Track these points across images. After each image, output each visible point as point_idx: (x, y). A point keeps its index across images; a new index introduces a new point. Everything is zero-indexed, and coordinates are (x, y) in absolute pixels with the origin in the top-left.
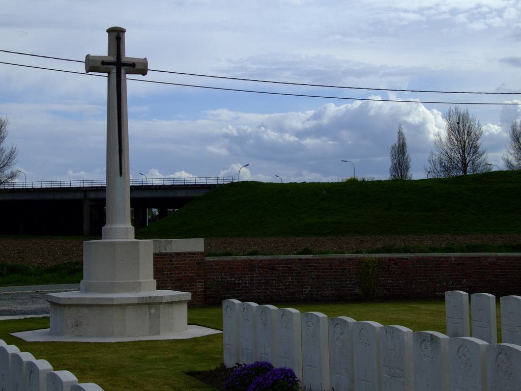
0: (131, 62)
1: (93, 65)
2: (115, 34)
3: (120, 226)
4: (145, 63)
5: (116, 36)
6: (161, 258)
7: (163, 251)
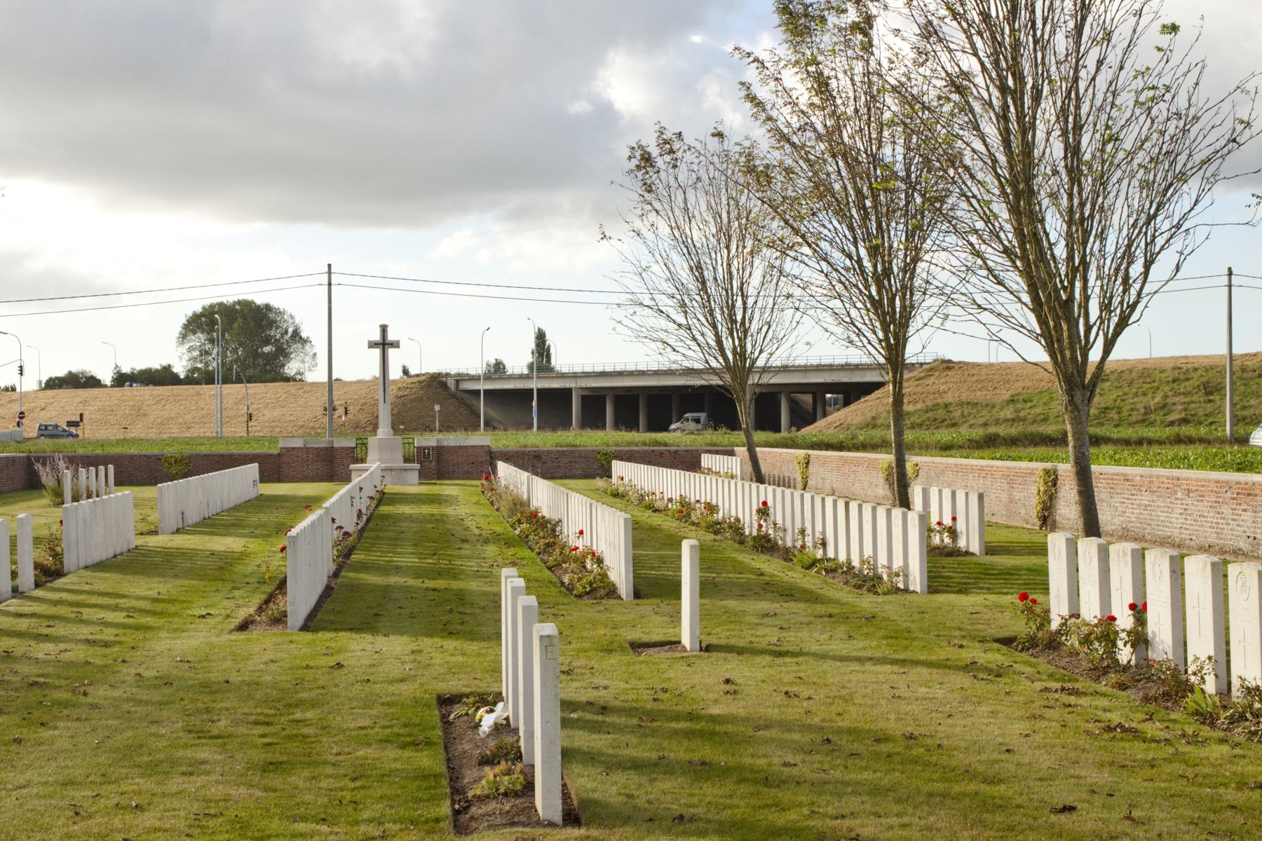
1: (372, 345)
5: (384, 329)
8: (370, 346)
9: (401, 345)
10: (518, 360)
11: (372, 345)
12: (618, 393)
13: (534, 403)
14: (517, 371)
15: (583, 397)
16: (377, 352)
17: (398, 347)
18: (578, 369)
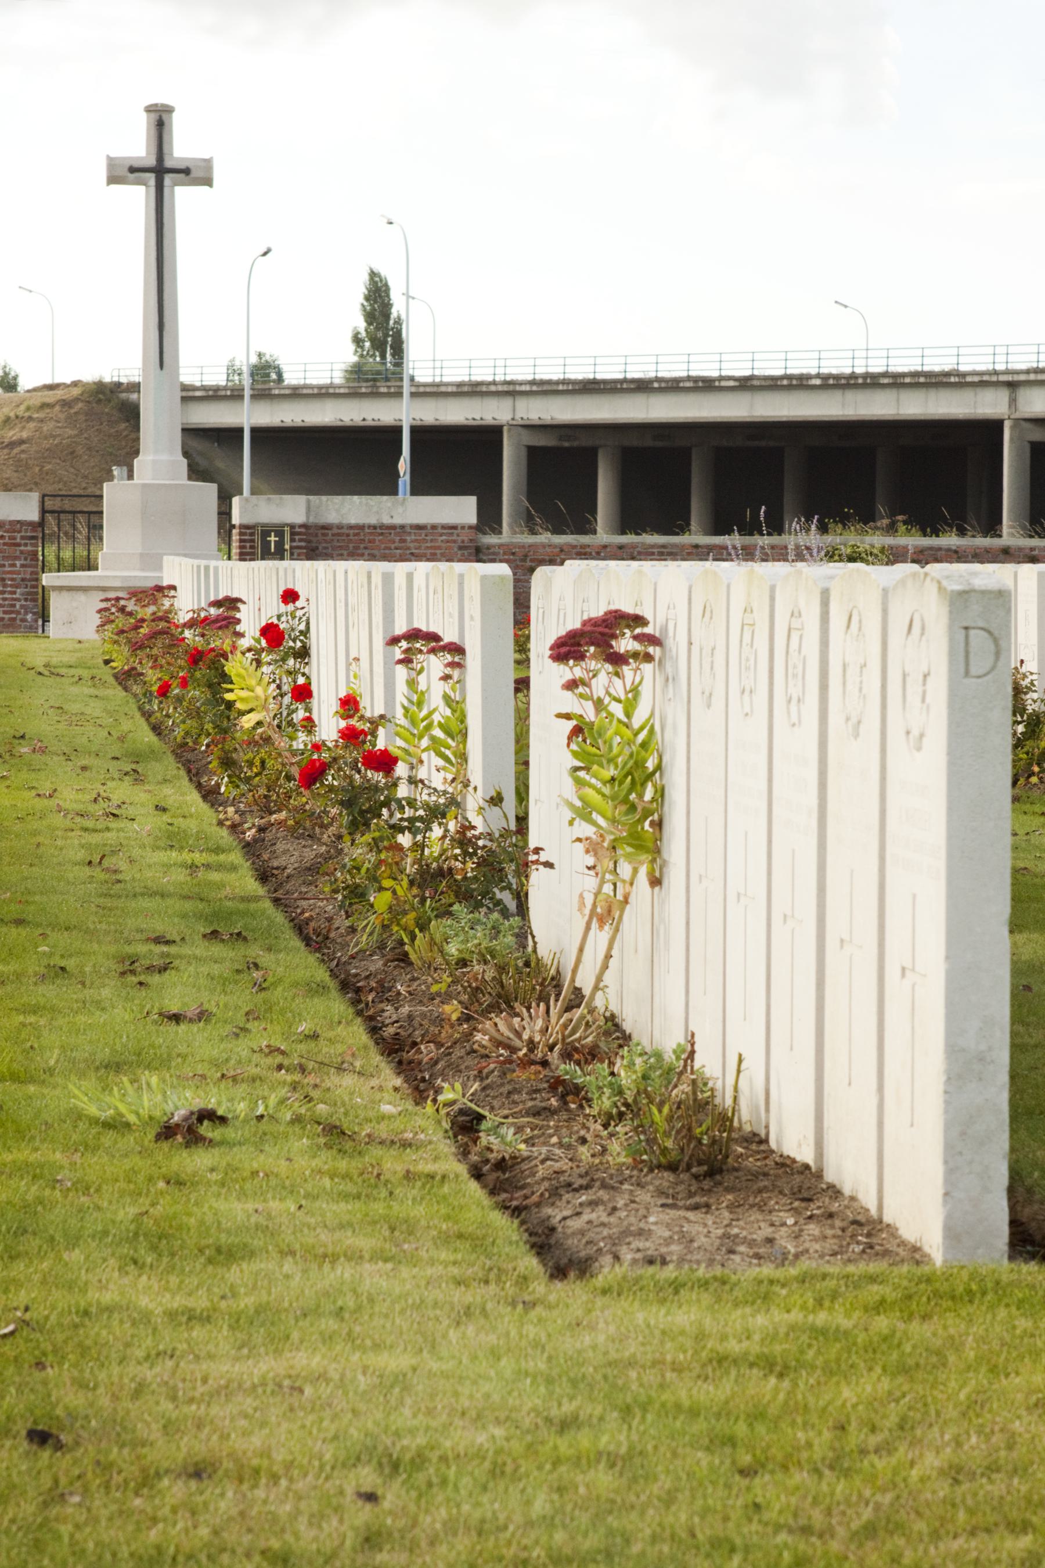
0: (182, 166)
1: (123, 173)
2: (154, 116)
3: (159, 457)
4: (207, 164)
5: (160, 120)
6: (382, 534)
7: (386, 520)
8: (113, 179)
9: (218, 175)
10: (319, 351)
11: (123, 173)
12: (634, 441)
13: (404, 465)
14: (318, 377)
15: (533, 452)
16: (137, 197)
17: (207, 181)
18: (521, 373)
